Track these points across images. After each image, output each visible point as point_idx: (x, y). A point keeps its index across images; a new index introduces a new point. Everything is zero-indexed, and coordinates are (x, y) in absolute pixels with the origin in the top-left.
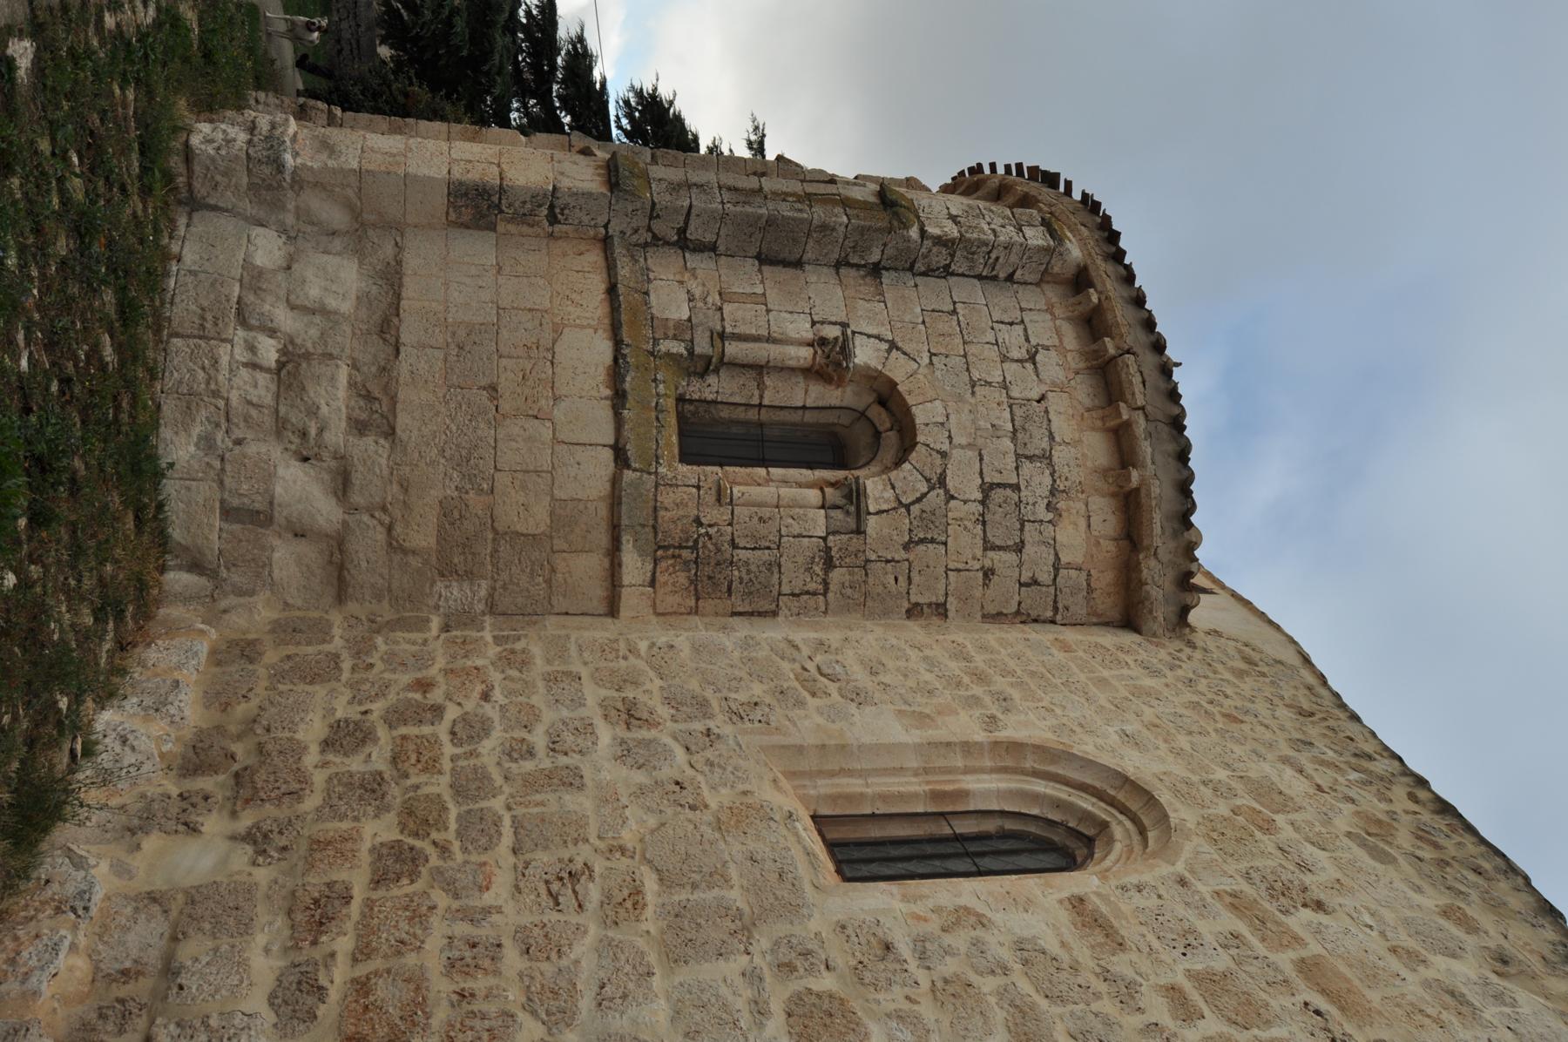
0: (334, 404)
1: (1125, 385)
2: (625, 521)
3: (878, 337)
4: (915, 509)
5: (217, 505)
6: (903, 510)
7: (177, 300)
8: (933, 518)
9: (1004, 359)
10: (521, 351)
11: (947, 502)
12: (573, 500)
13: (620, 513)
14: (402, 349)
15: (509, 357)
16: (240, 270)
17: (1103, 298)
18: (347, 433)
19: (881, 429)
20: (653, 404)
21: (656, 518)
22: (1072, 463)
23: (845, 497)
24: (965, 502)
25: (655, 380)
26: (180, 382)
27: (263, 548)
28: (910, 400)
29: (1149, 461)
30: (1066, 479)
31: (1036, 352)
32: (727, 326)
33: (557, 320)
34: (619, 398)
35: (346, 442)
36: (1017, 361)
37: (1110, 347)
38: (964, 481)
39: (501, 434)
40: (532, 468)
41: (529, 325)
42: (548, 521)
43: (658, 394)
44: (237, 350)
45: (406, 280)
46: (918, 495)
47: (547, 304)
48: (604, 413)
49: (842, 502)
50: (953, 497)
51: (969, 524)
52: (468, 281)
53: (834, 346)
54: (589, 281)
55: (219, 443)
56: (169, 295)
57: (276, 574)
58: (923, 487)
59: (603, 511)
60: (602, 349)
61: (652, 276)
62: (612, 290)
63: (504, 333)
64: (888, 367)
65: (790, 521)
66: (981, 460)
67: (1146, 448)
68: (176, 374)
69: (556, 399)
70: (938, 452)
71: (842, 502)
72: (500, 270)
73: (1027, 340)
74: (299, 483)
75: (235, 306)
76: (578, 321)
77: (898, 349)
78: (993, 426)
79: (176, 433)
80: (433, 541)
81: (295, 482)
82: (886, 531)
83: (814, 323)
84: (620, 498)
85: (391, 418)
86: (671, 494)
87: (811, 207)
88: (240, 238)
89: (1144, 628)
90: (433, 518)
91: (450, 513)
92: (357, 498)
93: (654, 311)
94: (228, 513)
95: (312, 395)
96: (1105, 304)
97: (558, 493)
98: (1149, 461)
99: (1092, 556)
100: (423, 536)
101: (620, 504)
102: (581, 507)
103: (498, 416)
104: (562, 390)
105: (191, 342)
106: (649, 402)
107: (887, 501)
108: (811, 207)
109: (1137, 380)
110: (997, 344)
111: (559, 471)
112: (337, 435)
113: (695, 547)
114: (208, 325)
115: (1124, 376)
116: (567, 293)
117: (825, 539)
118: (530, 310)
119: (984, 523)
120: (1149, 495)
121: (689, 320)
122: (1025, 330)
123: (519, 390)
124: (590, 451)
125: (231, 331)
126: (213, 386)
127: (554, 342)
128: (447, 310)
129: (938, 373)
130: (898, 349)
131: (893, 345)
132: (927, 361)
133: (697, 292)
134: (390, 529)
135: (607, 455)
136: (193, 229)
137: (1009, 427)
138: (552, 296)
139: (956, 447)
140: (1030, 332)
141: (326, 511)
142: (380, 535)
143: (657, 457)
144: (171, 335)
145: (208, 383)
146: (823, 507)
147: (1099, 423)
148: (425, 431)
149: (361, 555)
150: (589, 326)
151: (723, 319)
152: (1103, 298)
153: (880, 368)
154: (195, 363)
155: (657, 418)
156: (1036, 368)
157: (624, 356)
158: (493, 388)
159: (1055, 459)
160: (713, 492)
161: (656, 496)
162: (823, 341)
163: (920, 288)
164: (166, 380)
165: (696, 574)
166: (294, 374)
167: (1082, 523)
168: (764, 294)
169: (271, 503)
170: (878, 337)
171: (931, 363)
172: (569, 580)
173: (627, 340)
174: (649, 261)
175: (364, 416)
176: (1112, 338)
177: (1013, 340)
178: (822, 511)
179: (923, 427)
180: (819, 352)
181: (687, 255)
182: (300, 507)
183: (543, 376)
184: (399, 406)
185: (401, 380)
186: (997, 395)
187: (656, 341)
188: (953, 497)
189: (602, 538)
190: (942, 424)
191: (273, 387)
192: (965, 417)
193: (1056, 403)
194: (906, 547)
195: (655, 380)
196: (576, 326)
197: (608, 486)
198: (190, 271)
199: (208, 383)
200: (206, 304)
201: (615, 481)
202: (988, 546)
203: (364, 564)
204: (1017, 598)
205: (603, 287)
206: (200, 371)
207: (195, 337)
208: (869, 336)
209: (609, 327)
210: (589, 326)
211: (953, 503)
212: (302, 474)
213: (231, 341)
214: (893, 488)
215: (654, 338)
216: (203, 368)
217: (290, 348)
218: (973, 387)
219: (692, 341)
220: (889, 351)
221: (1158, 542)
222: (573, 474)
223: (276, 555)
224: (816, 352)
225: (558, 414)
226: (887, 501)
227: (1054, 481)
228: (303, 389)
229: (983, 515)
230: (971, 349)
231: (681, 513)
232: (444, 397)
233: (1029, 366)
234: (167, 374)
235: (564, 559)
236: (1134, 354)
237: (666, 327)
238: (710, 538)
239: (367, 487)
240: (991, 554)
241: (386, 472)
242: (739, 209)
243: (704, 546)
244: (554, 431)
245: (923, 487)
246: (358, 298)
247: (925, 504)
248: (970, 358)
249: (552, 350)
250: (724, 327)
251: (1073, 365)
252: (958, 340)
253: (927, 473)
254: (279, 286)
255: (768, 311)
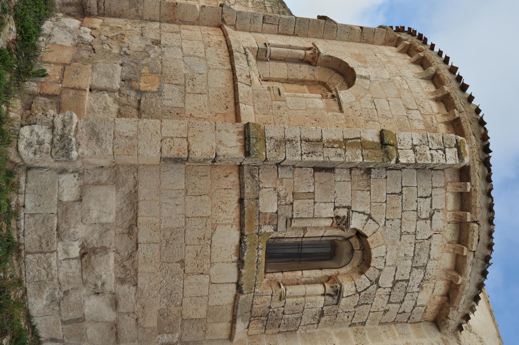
0: (108, 273)
1: (470, 240)
2: (239, 314)
3: (364, 213)
4: (363, 294)
5: (60, 321)
6: (358, 295)
7: (26, 233)
8: (369, 296)
9: (419, 219)
10: (196, 242)
11: (377, 289)
12: (216, 305)
13: (237, 312)
14: (139, 246)
15: (190, 245)
16: (56, 208)
17: (473, 189)
18: (116, 283)
19: (355, 249)
20: (256, 261)
21: (252, 308)
22: (434, 268)
23: (334, 292)
24: (384, 288)
25: (258, 248)
26: (34, 277)
27: (82, 329)
28: (371, 246)
29: (468, 275)
30: (430, 275)
31: (433, 214)
32: (294, 214)
33: (214, 222)
34: (240, 263)
35: (115, 287)
36: (424, 219)
37: (469, 217)
38: (386, 281)
39: (186, 282)
40: (199, 295)
41: (200, 227)
42: (206, 313)
43: (258, 256)
44: (60, 254)
45: (140, 204)
46: (365, 288)
47: (209, 213)
48: (233, 269)
49: (333, 293)
50: (380, 287)
51: (383, 296)
52: (170, 201)
53: (342, 220)
54: (230, 195)
55: (57, 296)
56: (22, 231)
57: (89, 337)
58: (368, 284)
59: (230, 308)
60: (235, 235)
61: (261, 186)
62: (241, 201)
63: (188, 232)
64: (365, 229)
65: (309, 303)
66: (396, 270)
67: (469, 269)
68: (31, 273)
69: (212, 264)
70: (378, 269)
71: (333, 293)
72: (187, 192)
73: (431, 207)
74: (95, 305)
75: (56, 232)
76: (224, 222)
77: (371, 218)
78: (405, 255)
79: (36, 299)
80: (155, 324)
81: (93, 305)
82: (348, 303)
83: (335, 208)
84: (237, 306)
85: (135, 278)
86: (260, 299)
87: (345, 150)
88: (54, 186)
89: (442, 331)
90: (155, 317)
91: (161, 314)
92: (121, 310)
93: (261, 209)
94: (64, 323)
95: (98, 270)
96: (473, 193)
97: (210, 304)
98: (468, 275)
99: (430, 302)
100: (152, 322)
101: (237, 308)
102: (220, 308)
103: (184, 275)
104: (214, 259)
105: (37, 256)
106: (254, 261)
107: (351, 292)
108: (345, 150)
109: (476, 239)
110: (417, 211)
111: (212, 295)
112: (111, 285)
113: (267, 315)
114: (44, 246)
115: (471, 235)
116: (219, 204)
117: (322, 308)
118: (201, 217)
119: (390, 295)
120: (463, 289)
121: (277, 212)
122: (432, 200)
123: (195, 262)
124: (226, 286)
125: (55, 246)
126: (50, 277)
127: (212, 234)
128: (160, 222)
129: (387, 230)
130: (371, 218)
131: (370, 217)
132: (383, 223)
133: (282, 194)
134: (137, 320)
135: (234, 287)
136: (29, 185)
137: (412, 255)
138: (212, 207)
139: (387, 266)
140: (433, 202)
141: (109, 315)
142: (133, 322)
143: (255, 285)
144: (27, 253)
145: (47, 276)
146: (324, 295)
147: (452, 250)
148: (151, 284)
149: (125, 330)
150: (229, 224)
151: (293, 210)
152: (473, 189)
153: (361, 229)
154: (40, 267)
155: (257, 267)
156: (431, 222)
157: (245, 242)
158: (182, 262)
159: (428, 267)
160: (278, 297)
161: (253, 300)
162: (337, 217)
163: (388, 179)
164: (27, 277)
165: (266, 324)
166: (89, 261)
167: (431, 291)
168: (314, 193)
169: (84, 315)
170: (364, 213)
171: (385, 225)
172: (213, 331)
173: (246, 233)
174: (261, 175)
175: (123, 276)
176: (471, 213)
177: (424, 208)
178: (323, 298)
179: (374, 259)
180: (335, 222)
181: (279, 169)
182: (97, 315)
183: (206, 253)
184: (139, 274)
185: (139, 262)
186: (411, 239)
187: (260, 227)
188: (380, 287)
189: (229, 318)
190: (383, 257)
191: (79, 266)
192: (395, 252)
193: (437, 240)
194: (355, 307)
195: (258, 248)
196: (223, 224)
197: (232, 299)
198: (30, 214)
199: (47, 276)
200: (41, 234)
201: (236, 298)
202: (389, 302)
203: (126, 333)
204: (395, 317)
205: (237, 198)
206: (43, 270)
207: (38, 253)
208: (359, 213)
209: (238, 223)
210: (229, 224)
211: (379, 289)
212: (96, 301)
213: (56, 251)
214: (356, 286)
215: (259, 225)
216: (44, 268)
217: (86, 244)
218: (401, 236)
219: (277, 225)
220: (367, 220)
221: (460, 306)
222: (217, 296)
223: (88, 331)
224: (333, 222)
225: (212, 271)
226: (351, 292)
227: (425, 276)
228: (93, 269)
229: (390, 292)
230: (405, 215)
231: (263, 305)
232: (160, 268)
233: (429, 222)
234: (27, 274)
235: (212, 325)
236: (479, 224)
237: (265, 218)
238: (274, 312)
239: (125, 305)
240: (389, 305)
241: (134, 301)
242: (309, 159)
243: (271, 315)
244: (210, 278)
245: (368, 284)
246: (117, 212)
247: (368, 291)
248: (403, 220)
249: (211, 239)
250: (292, 215)
251: (448, 220)
252: (400, 211)
253: (371, 279)
254: (77, 214)
255: (315, 203)
